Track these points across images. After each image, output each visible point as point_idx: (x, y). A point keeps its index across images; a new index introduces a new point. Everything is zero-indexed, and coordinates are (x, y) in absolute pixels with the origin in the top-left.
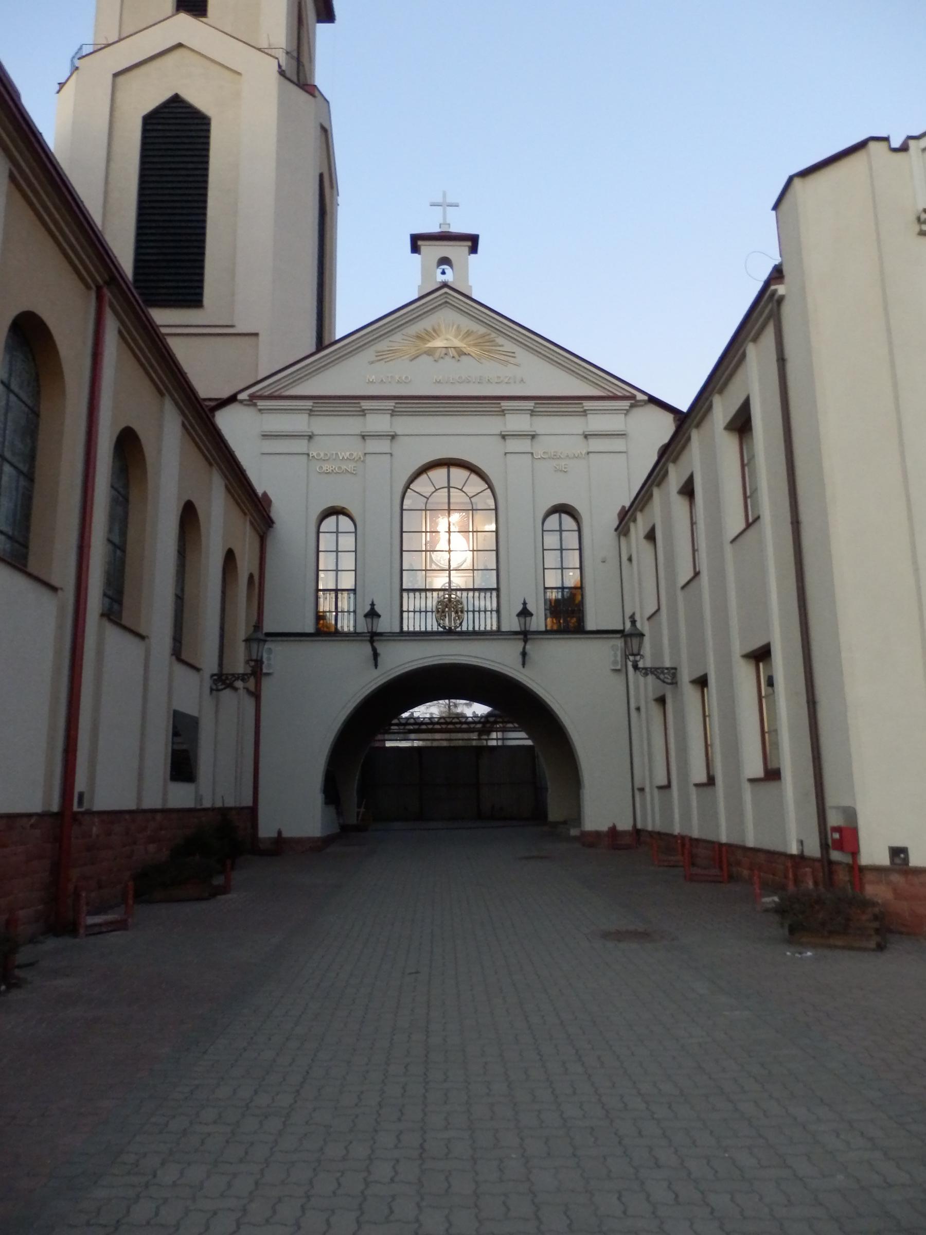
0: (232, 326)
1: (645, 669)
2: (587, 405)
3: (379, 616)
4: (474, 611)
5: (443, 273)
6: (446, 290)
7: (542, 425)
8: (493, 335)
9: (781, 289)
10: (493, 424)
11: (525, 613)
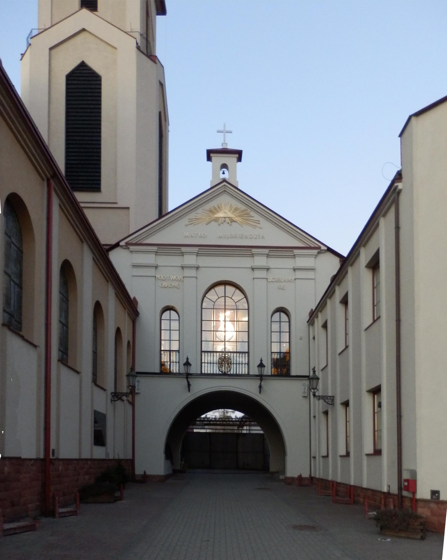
0: (116, 203)
1: (319, 396)
2: (296, 252)
3: (191, 365)
4: (236, 364)
5: (224, 173)
6: (225, 183)
7: (273, 263)
8: (249, 210)
9: (400, 186)
10: (247, 262)
11: (261, 365)
